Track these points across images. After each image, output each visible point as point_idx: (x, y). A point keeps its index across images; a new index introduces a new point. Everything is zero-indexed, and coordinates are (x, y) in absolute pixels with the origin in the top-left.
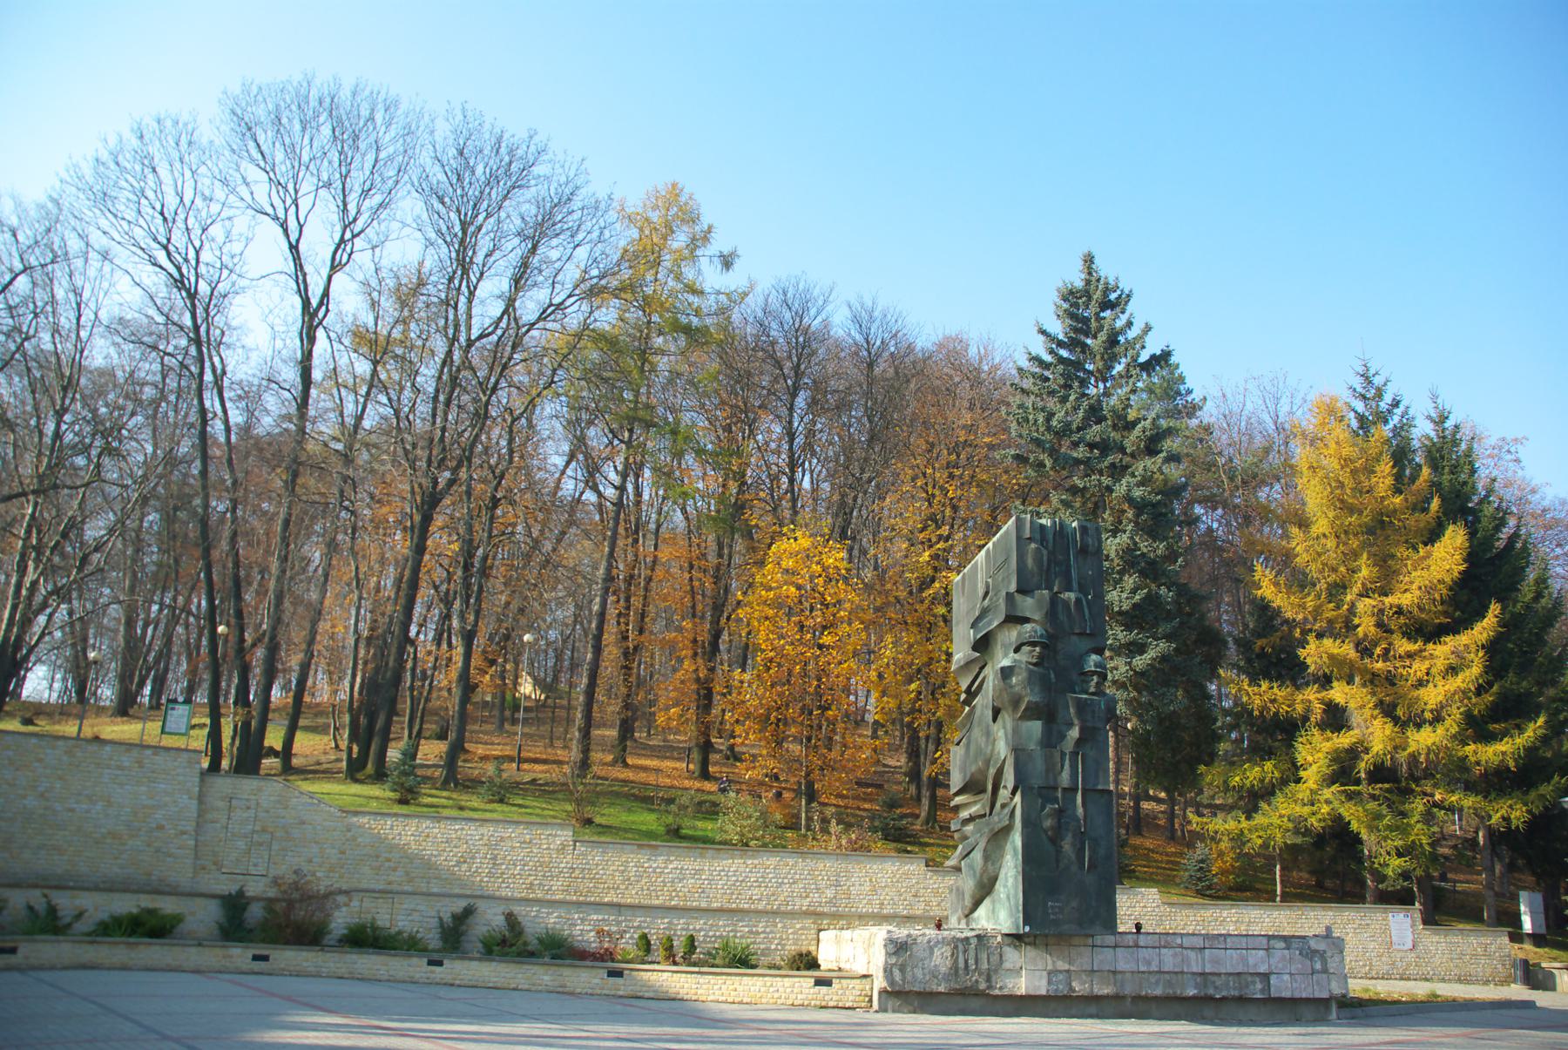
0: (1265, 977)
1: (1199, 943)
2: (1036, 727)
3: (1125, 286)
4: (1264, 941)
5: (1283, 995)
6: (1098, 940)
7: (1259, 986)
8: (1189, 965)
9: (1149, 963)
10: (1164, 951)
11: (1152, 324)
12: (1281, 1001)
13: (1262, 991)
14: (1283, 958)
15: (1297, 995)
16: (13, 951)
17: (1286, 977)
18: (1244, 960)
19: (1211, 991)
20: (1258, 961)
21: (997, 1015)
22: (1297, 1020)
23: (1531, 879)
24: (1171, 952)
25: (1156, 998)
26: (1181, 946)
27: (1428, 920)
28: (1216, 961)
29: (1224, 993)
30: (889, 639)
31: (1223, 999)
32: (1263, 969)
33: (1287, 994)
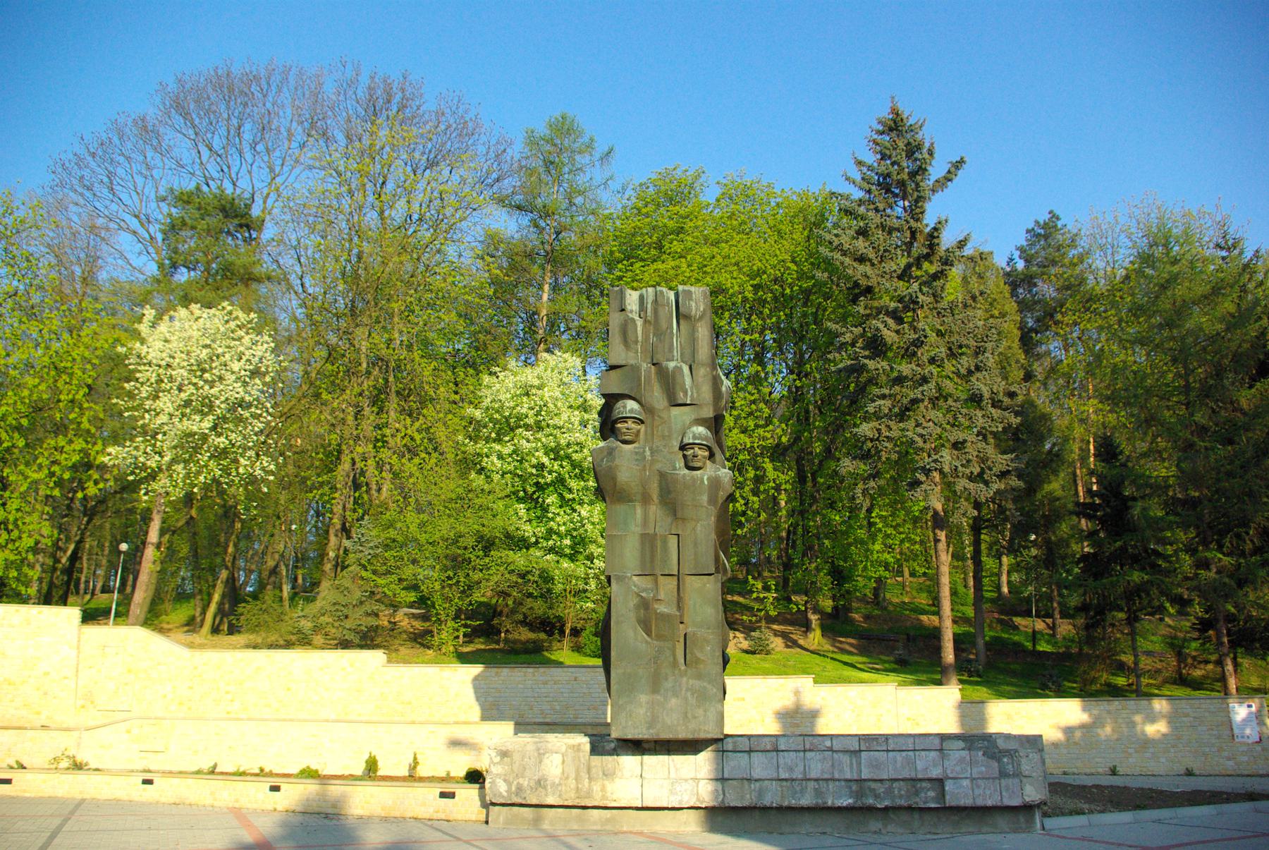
0: (940, 782)
3: (557, 114)
4: (937, 741)
7: (931, 794)
8: (841, 771)
9: (791, 769)
10: (809, 754)
12: (951, 808)
13: (935, 799)
14: (962, 760)
15: (980, 802)
16: (8, 781)
17: (966, 783)
18: (911, 763)
19: (870, 801)
20: (928, 766)
22: (427, 784)
23: (891, 608)
24: (818, 756)
25: (839, 809)
26: (831, 749)
27: (815, 682)
28: (876, 766)
29: (887, 803)
31: (886, 809)
32: (935, 773)
33: (967, 802)
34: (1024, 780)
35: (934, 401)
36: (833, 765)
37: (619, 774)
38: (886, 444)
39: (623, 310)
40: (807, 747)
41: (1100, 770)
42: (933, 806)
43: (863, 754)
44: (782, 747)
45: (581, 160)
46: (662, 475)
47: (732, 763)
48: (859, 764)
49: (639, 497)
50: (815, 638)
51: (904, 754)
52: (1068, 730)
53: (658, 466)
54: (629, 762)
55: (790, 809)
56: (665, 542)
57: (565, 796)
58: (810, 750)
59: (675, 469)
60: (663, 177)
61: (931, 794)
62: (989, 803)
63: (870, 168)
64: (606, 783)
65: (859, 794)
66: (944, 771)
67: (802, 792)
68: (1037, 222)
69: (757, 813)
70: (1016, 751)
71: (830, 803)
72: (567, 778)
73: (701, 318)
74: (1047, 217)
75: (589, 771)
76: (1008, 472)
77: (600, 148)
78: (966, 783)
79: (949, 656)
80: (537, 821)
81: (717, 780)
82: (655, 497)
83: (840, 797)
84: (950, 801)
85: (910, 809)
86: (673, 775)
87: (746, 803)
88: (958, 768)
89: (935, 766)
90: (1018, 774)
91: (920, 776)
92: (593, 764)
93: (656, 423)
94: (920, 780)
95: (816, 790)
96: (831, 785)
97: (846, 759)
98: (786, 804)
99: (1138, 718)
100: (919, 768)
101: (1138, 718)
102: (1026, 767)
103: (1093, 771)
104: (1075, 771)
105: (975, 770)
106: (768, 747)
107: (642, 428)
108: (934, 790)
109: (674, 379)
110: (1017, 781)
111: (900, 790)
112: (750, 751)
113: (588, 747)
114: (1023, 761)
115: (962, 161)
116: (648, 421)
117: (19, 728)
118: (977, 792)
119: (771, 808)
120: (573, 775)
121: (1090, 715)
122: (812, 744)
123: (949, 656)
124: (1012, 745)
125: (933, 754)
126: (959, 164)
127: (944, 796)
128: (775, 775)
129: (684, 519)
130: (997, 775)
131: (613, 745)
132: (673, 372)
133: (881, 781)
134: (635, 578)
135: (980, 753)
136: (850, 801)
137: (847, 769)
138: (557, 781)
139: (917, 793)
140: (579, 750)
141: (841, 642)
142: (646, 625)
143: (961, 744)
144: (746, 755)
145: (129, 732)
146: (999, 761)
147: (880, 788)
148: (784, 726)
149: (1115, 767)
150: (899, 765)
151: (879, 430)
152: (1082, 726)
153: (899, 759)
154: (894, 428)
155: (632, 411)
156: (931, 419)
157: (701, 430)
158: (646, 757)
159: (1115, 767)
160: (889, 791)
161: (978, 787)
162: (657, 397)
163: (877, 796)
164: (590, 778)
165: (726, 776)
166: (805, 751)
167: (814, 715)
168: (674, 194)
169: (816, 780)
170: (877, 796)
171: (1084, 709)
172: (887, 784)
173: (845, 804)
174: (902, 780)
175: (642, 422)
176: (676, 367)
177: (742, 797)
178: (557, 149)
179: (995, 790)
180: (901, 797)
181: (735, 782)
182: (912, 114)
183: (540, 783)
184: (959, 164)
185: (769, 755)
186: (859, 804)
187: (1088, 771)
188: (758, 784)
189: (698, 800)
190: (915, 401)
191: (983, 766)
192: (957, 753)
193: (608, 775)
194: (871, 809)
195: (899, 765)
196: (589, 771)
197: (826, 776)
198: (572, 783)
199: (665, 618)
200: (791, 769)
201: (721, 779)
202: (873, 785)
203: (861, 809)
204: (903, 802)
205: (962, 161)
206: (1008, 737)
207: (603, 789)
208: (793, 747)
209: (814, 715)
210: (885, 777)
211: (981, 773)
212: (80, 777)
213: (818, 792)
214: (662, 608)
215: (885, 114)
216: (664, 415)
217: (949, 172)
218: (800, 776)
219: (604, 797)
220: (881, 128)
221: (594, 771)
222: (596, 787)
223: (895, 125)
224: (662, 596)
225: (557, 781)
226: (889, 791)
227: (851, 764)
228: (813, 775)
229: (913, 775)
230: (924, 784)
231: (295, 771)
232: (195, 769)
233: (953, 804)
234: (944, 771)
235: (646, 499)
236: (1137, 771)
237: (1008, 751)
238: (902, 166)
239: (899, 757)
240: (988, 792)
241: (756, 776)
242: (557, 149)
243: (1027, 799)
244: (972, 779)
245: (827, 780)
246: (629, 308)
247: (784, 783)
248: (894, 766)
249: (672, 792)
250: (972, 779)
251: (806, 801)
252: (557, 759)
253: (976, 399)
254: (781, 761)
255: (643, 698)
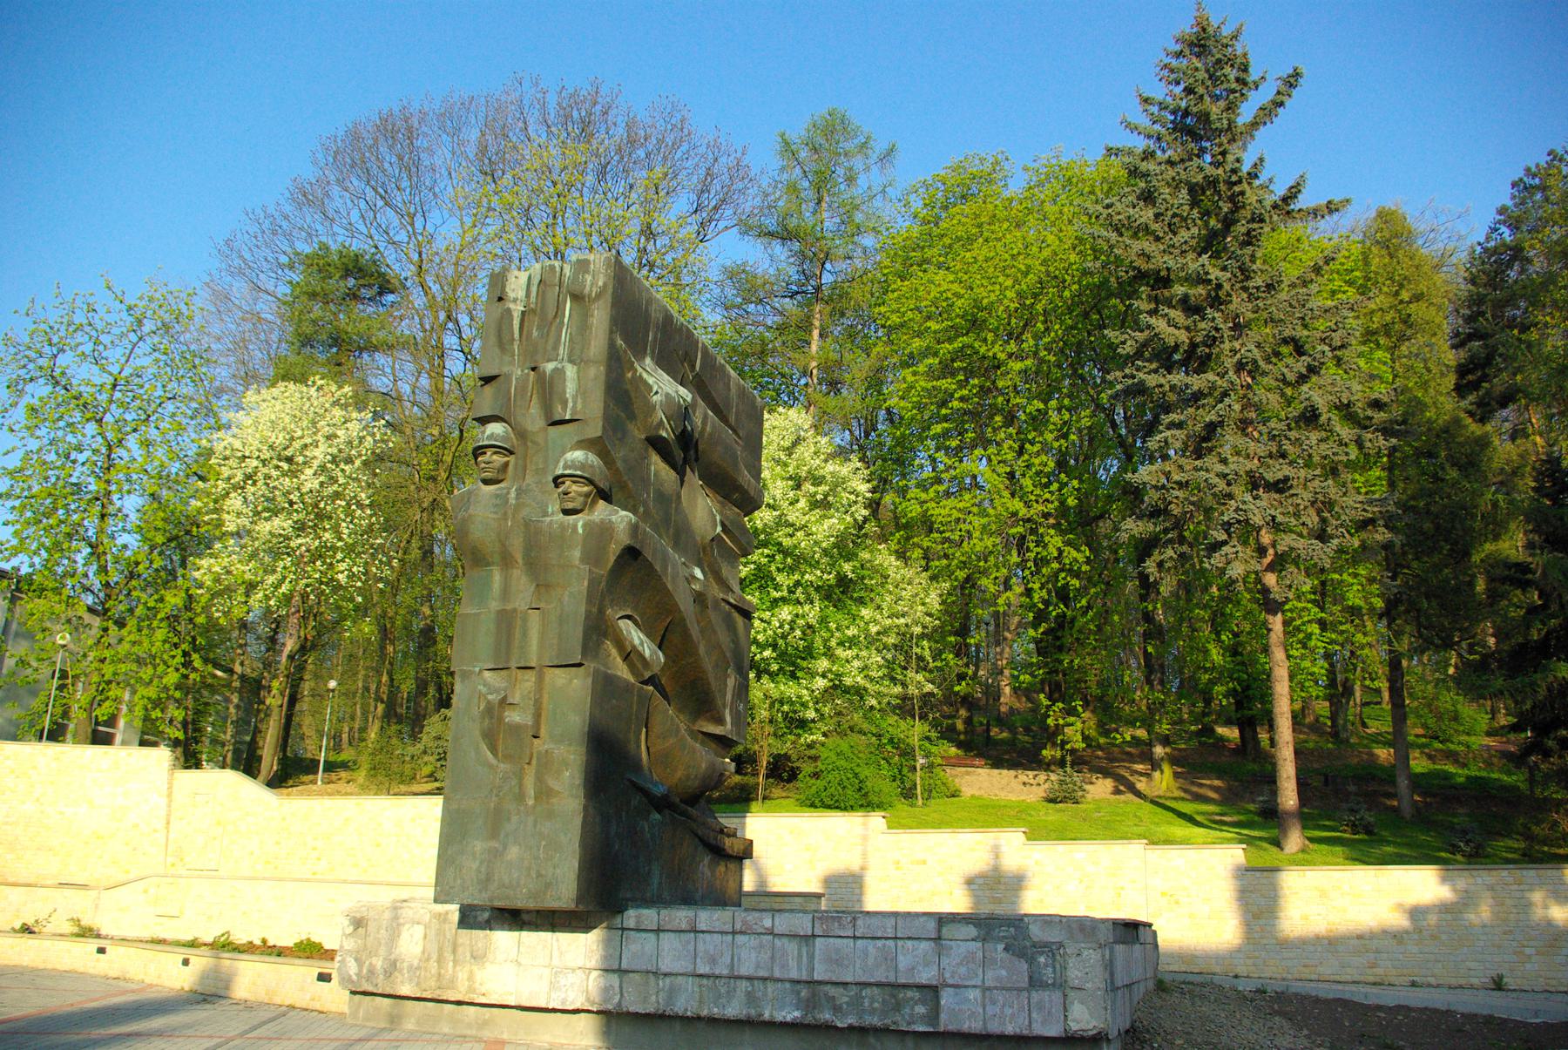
0: (931, 991)
1: (803, 924)
2: (15, 542)
4: (932, 925)
5: (966, 1027)
6: (631, 916)
7: (921, 1009)
8: (784, 966)
9: (713, 961)
10: (740, 939)
11: (1303, 70)
14: (969, 958)
17: (973, 994)
19: (826, 1016)
20: (916, 964)
21: (908, 915)
24: (753, 941)
25: (784, 1025)
28: (836, 961)
29: (851, 1020)
30: (998, 541)
31: (851, 1028)
32: (926, 976)
34: (1072, 994)
35: (1243, 425)
36: (773, 957)
37: (490, 956)
38: (1176, 493)
39: (500, 299)
40: (738, 927)
41: (1475, 981)
42: (921, 1029)
43: (818, 940)
44: (702, 926)
45: (858, 163)
46: (527, 524)
47: (633, 947)
48: (811, 957)
49: (497, 558)
50: (1163, 781)
51: (880, 943)
52: (1416, 913)
53: (525, 512)
54: (504, 939)
55: (713, 1021)
56: (525, 620)
57: (424, 986)
58: (741, 932)
59: (545, 514)
60: (957, 168)
61: (921, 1009)
62: (1010, 1029)
63: (1163, 106)
64: (475, 968)
65: (810, 1004)
66: (941, 971)
67: (730, 994)
68: (1528, 170)
69: (678, 1026)
70: (1061, 945)
71: (766, 1016)
72: (428, 960)
73: (599, 296)
74: (1543, 160)
75: (454, 951)
76: (1372, 521)
77: (879, 147)
78: (973, 994)
79: (1289, 797)
80: (394, 1020)
81: (606, 970)
82: (519, 557)
83: (781, 1008)
84: (946, 1023)
85: (885, 1031)
86: (555, 962)
87: (651, 1009)
88: (963, 970)
89: (927, 965)
90: (1061, 985)
91: (902, 981)
92: (460, 941)
93: (530, 452)
94: (905, 986)
95: (749, 994)
96: (770, 986)
97: (792, 947)
98: (705, 1013)
99: (1537, 896)
100: (901, 966)
101: (1537, 896)
102: (1074, 974)
103: (1462, 982)
104: (1432, 980)
105: (990, 974)
106: (683, 926)
107: (511, 459)
108: (923, 1002)
109: (551, 386)
110: (1057, 996)
111: (873, 1000)
112: (658, 931)
113: (456, 917)
114: (1071, 962)
115: (1296, 74)
116: (519, 451)
117: (29, 885)
118: (990, 1010)
119: (699, 1018)
120: (435, 957)
121: (1455, 891)
122: (744, 922)
123: (1289, 797)
124: (1053, 936)
125: (924, 945)
126: (1292, 80)
127: (938, 1014)
128: (690, 968)
129: (548, 586)
130: (1025, 983)
131: (486, 915)
132: (552, 377)
133: (845, 984)
134: (487, 674)
135: (1001, 947)
136: (797, 1014)
137: (793, 963)
138: (416, 963)
139: (898, 1007)
140: (445, 921)
141: (1201, 785)
142: (490, 738)
143: (972, 931)
144: (652, 936)
145: (145, 891)
146: (1031, 961)
147: (843, 997)
148: (977, 900)
149: (1501, 977)
150: (871, 961)
151: (1167, 475)
152: (1444, 908)
153: (870, 948)
154: (1187, 468)
155: (491, 437)
156: (1238, 452)
157: (578, 455)
158: (524, 934)
159: (1501, 977)
160: (856, 1002)
161: (994, 1003)
162: (533, 418)
163: (837, 1009)
164: (455, 962)
165: (624, 966)
166: (734, 933)
167: (1017, 883)
168: (965, 189)
169: (749, 978)
170: (837, 1009)
171: (1444, 880)
172: (853, 990)
173: (789, 1018)
174: (878, 985)
175: (511, 453)
176: (556, 370)
177: (645, 1000)
178: (824, 155)
179: (1021, 1009)
180: (873, 1012)
181: (637, 976)
182: (1222, 19)
183: (392, 967)
184: (1292, 80)
185: (685, 937)
186: (809, 1020)
187: (1453, 982)
188: (668, 980)
189: (588, 999)
190: (1211, 428)
191: (1004, 968)
192: (963, 944)
193: (478, 957)
194: (828, 1028)
195: (871, 961)
196: (454, 951)
197: (762, 973)
198: (433, 965)
199: (516, 729)
200: (713, 961)
201: (614, 968)
202: (832, 991)
203: (808, 1026)
204: (875, 1021)
205: (1296, 74)
206: (1048, 920)
207: (471, 978)
208: (718, 926)
209: (1017, 883)
210: (849, 979)
211: (999, 979)
212: (26, 941)
213: (751, 998)
214: (514, 717)
215: (1187, 27)
216: (540, 439)
217: (1279, 93)
218: (725, 972)
219: (471, 989)
220: (1178, 48)
221: (460, 950)
222: (462, 975)
223: (1200, 43)
224: (516, 698)
225: (416, 963)
226: (856, 1002)
227: (800, 955)
228: (744, 971)
229: (892, 979)
230: (910, 994)
231: (288, 941)
232: (188, 937)
233: (951, 1028)
234: (941, 971)
235: (507, 561)
236: (1540, 984)
237: (1046, 945)
238: (1208, 91)
239: (871, 946)
240: (1008, 1011)
241: (664, 968)
242: (824, 155)
243: (1074, 1027)
244: (985, 990)
245: (765, 979)
246: (512, 295)
247: (705, 981)
248: (863, 963)
249: (553, 986)
250: (985, 990)
251: (733, 1010)
252: (419, 931)
253: (1310, 417)
254: (701, 947)
255: (479, 846)
